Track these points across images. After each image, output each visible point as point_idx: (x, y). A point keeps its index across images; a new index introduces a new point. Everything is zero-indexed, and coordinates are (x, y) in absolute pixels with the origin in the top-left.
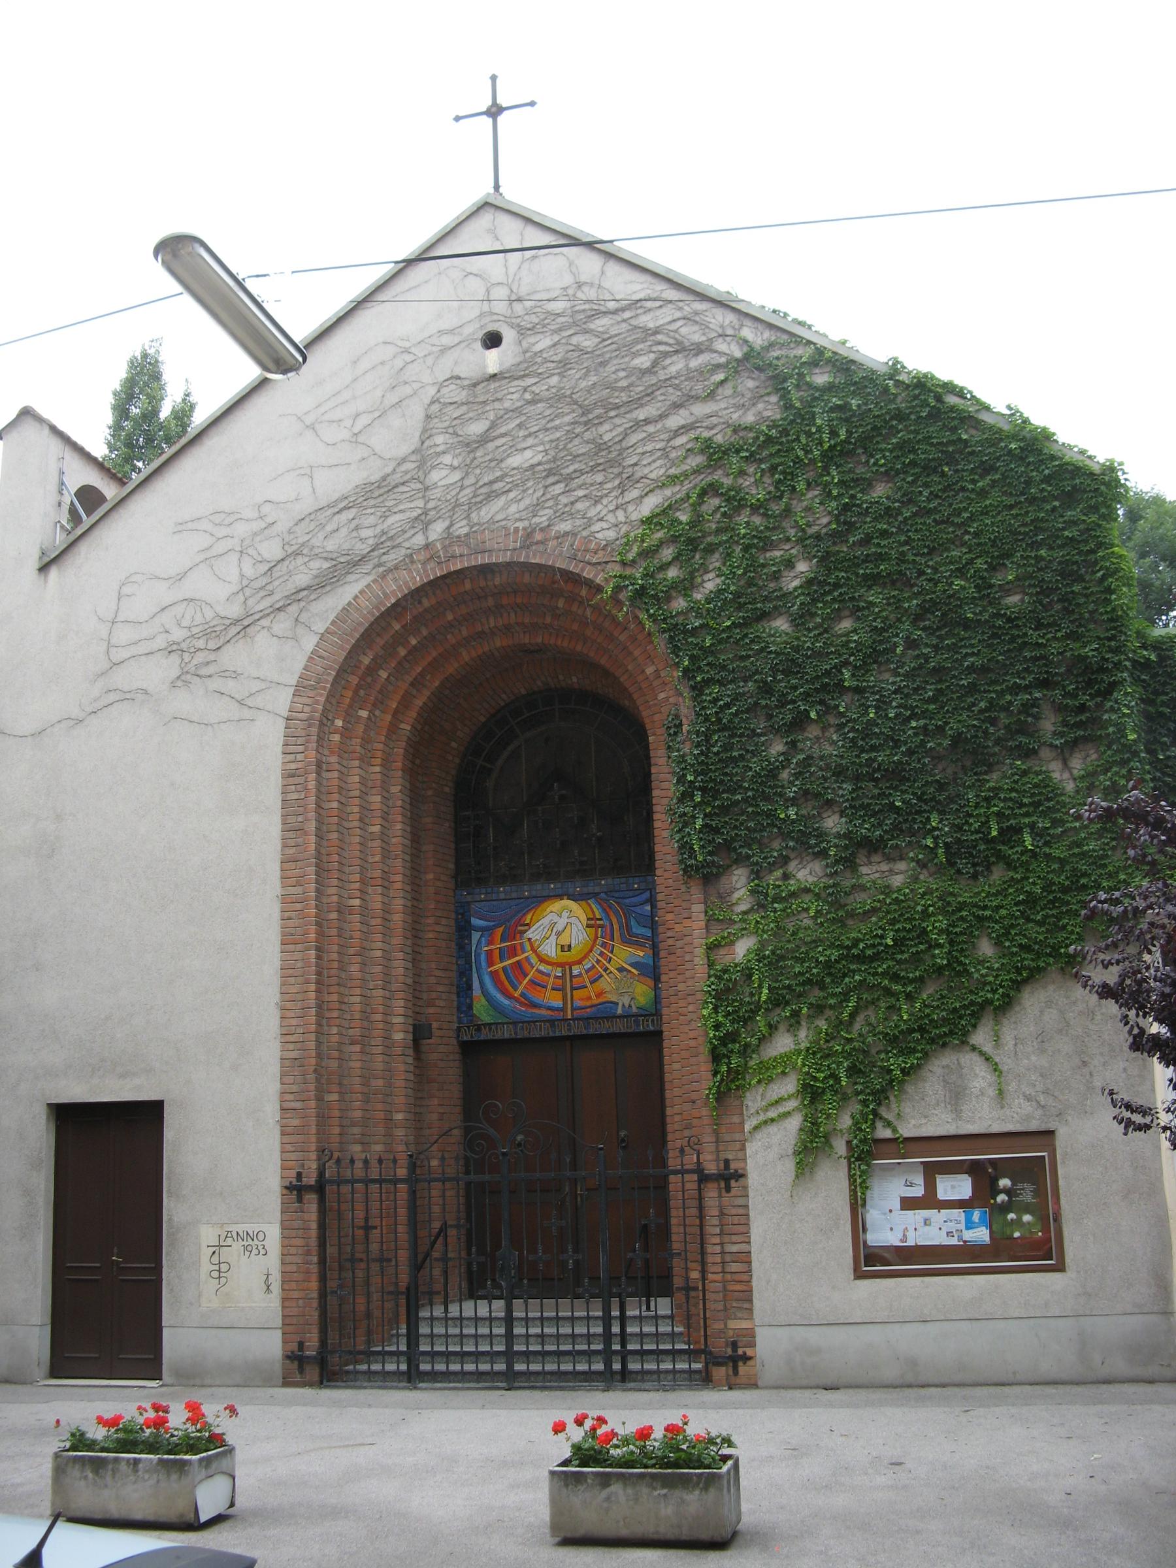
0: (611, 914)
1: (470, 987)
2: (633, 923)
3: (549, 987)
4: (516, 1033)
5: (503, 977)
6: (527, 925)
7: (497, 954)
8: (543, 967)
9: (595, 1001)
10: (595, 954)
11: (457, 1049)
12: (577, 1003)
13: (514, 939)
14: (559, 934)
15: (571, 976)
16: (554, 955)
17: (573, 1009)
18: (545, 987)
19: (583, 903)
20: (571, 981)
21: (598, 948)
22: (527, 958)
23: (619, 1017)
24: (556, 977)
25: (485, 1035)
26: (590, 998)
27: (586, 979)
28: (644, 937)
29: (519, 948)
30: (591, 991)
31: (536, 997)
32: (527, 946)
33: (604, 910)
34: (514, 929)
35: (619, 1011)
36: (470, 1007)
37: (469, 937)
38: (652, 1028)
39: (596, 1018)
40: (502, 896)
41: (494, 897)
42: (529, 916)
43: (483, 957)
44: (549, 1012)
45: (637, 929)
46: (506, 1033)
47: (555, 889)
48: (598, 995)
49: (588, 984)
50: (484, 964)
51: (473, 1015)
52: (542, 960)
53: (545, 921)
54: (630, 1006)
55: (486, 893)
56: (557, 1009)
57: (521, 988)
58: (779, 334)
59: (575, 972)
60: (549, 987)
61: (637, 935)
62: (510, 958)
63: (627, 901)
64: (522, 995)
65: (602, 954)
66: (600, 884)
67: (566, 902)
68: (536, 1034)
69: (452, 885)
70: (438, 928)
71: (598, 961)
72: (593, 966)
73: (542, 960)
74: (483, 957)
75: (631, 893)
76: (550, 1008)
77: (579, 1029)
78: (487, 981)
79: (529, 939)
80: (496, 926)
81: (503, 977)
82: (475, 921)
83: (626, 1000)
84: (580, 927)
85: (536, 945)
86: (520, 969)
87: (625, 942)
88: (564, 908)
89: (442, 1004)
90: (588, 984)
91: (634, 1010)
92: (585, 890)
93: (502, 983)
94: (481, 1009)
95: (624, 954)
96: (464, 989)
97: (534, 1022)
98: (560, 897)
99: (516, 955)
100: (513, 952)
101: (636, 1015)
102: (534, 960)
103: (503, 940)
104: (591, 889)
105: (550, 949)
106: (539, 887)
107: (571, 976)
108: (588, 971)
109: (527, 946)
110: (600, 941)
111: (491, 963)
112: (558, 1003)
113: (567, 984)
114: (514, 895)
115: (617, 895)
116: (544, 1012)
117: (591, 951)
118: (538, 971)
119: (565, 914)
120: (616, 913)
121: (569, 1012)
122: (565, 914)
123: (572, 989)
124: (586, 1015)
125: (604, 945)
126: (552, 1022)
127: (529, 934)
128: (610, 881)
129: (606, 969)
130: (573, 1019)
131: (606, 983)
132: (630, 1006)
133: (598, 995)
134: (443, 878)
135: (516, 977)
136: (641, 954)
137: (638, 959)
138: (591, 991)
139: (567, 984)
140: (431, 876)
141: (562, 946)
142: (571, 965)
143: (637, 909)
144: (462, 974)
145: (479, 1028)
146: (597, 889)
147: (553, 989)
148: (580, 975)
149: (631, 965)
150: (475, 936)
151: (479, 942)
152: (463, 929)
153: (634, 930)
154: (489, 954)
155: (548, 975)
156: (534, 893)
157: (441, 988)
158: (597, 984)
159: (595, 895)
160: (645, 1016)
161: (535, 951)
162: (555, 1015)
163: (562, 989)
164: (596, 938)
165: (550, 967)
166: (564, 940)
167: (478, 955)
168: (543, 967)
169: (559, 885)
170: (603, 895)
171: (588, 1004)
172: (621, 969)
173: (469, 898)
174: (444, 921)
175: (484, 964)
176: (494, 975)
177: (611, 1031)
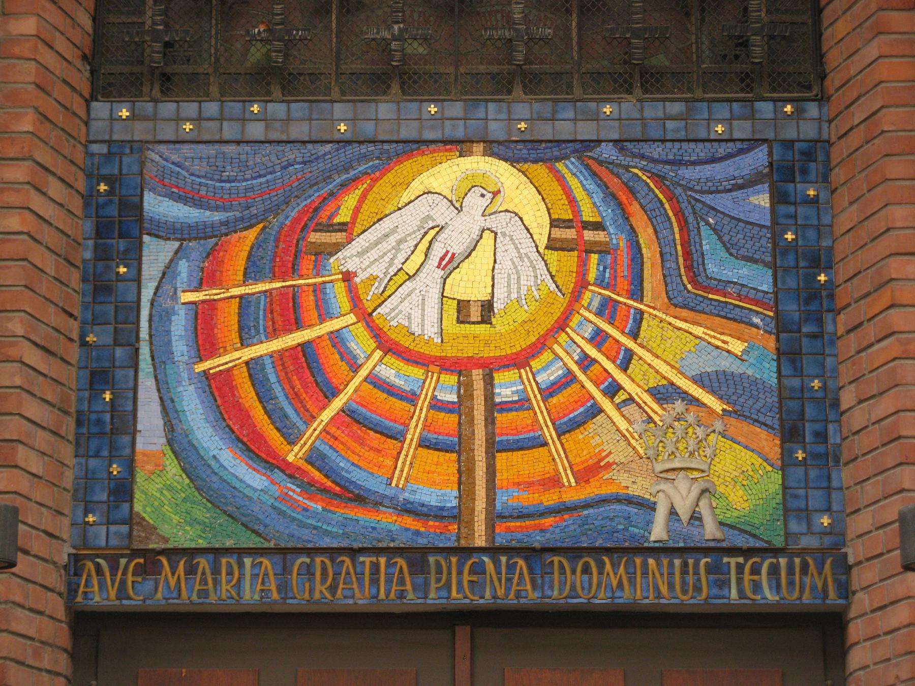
0: (635, 208)
1: (124, 423)
2: (708, 243)
3: (413, 434)
4: (283, 587)
5: (247, 395)
6: (343, 227)
7: (229, 319)
8: (392, 371)
9: (573, 492)
10: (578, 337)
11: (63, 637)
12: (505, 499)
13: (293, 270)
14: (450, 264)
15: (493, 407)
16: (431, 331)
17: (494, 517)
18: (398, 437)
19: (540, 170)
20: (490, 421)
21: (587, 319)
22: (336, 338)
23: (661, 551)
24: (437, 405)
25: (168, 590)
26: (554, 481)
27: (543, 417)
28: (744, 292)
29: (309, 300)
30: (558, 457)
31: (361, 467)
32: (339, 296)
33: (611, 196)
34: (297, 239)
35: (658, 532)
36: (123, 490)
37: (134, 256)
38: (770, 595)
39: (573, 552)
40: (256, 130)
41: (230, 130)
42: (350, 201)
43: (179, 325)
44: (574, 183)
45: (720, 265)
46: (251, 587)
47: (441, 119)
48: (585, 474)
49: (550, 433)
50: (181, 348)
51: (132, 520)
52: (388, 346)
53: (406, 221)
54: (695, 517)
55: (198, 120)
56: (438, 514)
57: (311, 435)
58: (217, 147)
59: (505, 391)
60: (413, 434)
61: (721, 287)
62: (274, 333)
63: (688, 173)
64: (315, 458)
65: (598, 339)
66: (596, 117)
67: (478, 163)
68: (357, 596)
69: (81, 79)
70: (37, 202)
71: (586, 362)
72: (569, 379)
73: (388, 346)
74: (179, 325)
75: (700, 151)
76: (409, 509)
77: (508, 587)
78: (193, 405)
79: (348, 277)
80: (231, 227)
81: (247, 395)
82: (157, 206)
83: (682, 495)
84: (527, 246)
85: (368, 298)
86: (309, 372)
87: (677, 302)
88: (472, 184)
89: (35, 465)
90: (550, 433)
91: (710, 530)
92: (545, 131)
93: (245, 416)
94: (163, 502)
95: (675, 346)
96: (103, 430)
97: (353, 552)
98: (460, 145)
99: (298, 325)
100: (288, 312)
101: (718, 550)
102: (361, 342)
103: (251, 273)
104: (564, 129)
105: (417, 312)
106: (385, 109)
107: (493, 407)
108: (548, 392)
109: (339, 296)
110: (592, 296)
111: (206, 342)
112: (446, 496)
113: (476, 430)
114: (299, 131)
115: (657, 151)
116: (388, 522)
117: (561, 325)
118: (374, 380)
119: (475, 202)
120: (654, 215)
121: (480, 527)
122: (475, 202)
123: (493, 448)
124: (538, 540)
125: (607, 309)
126: (417, 557)
127: (349, 258)
128: (629, 107)
129: (613, 389)
130: (493, 551)
131: (614, 433)
132: (695, 517)
133: (585, 474)
134: (61, 45)
135: (295, 397)
136: (737, 347)
137: (725, 364)
138: (558, 457)
139: (476, 430)
140: (27, 26)
141: (462, 306)
142: (489, 368)
143: (723, 202)
144: (99, 378)
145: (150, 561)
146: (586, 131)
147: (424, 444)
148: (522, 404)
149: (698, 380)
150: (156, 254)
151: (169, 272)
152: (117, 226)
153: (712, 268)
154: (204, 318)
155: (411, 398)
156: (368, 128)
157: (33, 410)
158: (579, 435)
159: (583, 148)
160: (748, 552)
161: (366, 317)
162: (428, 533)
163: (458, 447)
164: (582, 284)
165: (417, 372)
166: (470, 283)
167: (160, 317)
168: (392, 371)
169: (456, 109)
170: (607, 151)
171: (550, 499)
172: (664, 394)
173: (139, 131)
174: (55, 189)
175: (181, 348)
176: (218, 388)
177: (626, 597)
